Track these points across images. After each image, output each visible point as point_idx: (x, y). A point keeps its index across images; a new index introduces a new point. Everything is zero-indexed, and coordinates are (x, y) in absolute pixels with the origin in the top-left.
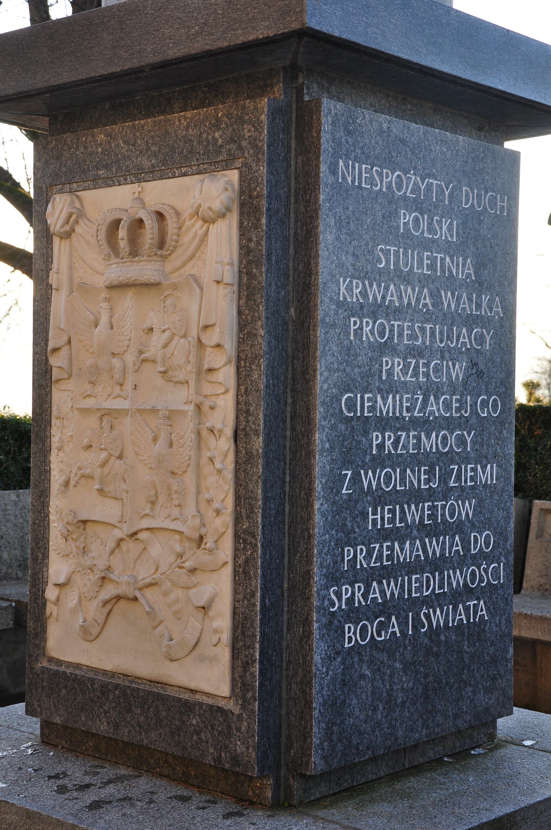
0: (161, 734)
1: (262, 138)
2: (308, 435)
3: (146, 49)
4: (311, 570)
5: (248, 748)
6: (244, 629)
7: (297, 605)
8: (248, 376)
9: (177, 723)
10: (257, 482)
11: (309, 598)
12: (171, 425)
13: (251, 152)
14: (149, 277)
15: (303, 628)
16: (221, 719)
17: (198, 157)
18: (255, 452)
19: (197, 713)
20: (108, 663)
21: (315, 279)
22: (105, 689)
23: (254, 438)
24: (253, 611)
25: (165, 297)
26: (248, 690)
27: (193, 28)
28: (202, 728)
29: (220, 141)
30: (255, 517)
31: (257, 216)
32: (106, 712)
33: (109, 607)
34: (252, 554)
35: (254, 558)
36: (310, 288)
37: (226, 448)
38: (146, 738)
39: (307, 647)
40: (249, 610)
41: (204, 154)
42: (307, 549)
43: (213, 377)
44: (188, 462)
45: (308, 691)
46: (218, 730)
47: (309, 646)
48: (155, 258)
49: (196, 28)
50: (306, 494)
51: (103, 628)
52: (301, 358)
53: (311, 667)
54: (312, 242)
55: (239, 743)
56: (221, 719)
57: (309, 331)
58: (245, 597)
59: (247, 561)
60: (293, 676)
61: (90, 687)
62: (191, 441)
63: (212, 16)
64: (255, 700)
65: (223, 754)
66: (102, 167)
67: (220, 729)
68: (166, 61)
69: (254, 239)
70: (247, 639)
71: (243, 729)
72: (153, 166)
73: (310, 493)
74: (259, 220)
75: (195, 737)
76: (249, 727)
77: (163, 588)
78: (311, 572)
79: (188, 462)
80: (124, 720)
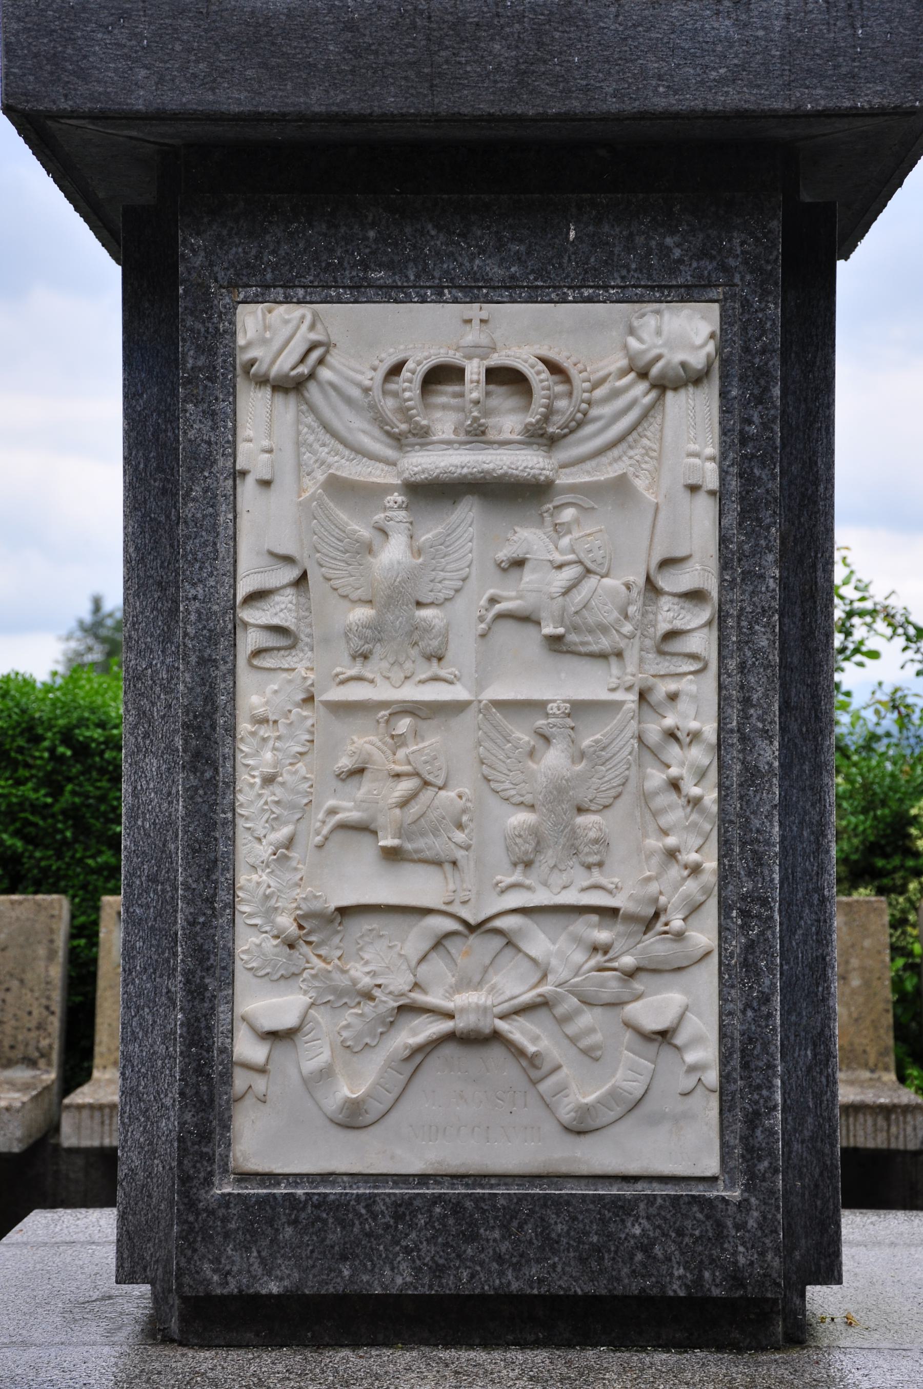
0: (554, 1266)
1: (772, 257)
2: (815, 739)
3: (601, 87)
4: (828, 954)
5: (762, 1254)
6: (747, 1059)
7: (800, 1014)
8: (747, 643)
9: (595, 1239)
10: (769, 816)
11: (824, 1000)
12: (572, 728)
13: (748, 277)
14: (537, 472)
15: (814, 1050)
16: (699, 1216)
17: (624, 272)
18: (764, 768)
19: (642, 1214)
20: (413, 1160)
21: (826, 489)
22: (403, 1210)
23: (762, 744)
24: (767, 1026)
25: (555, 508)
26: (760, 1159)
27: (714, 69)
28: (656, 1238)
29: (677, 253)
30: (766, 872)
31: (763, 382)
32: (407, 1251)
33: (418, 1058)
34: (762, 933)
35: (767, 940)
36: (815, 503)
37: (706, 762)
38: (517, 1279)
39: (824, 1080)
40: (759, 1026)
41: (639, 270)
42: (818, 921)
43: (678, 646)
44: (620, 789)
45: (827, 1150)
46: (692, 1235)
47: (828, 1076)
48: (540, 441)
49: (722, 71)
50: (813, 833)
51: (397, 1100)
52: (799, 614)
53: (833, 1110)
54: (819, 429)
55: (741, 1249)
56: (699, 1216)
57: (815, 572)
58: (748, 1006)
59: (750, 946)
60: (795, 1130)
61: (363, 1211)
62: (630, 754)
63: (758, 57)
64: (776, 1171)
65: (707, 1274)
66: (380, 266)
67: (697, 1233)
68: (646, 112)
69: (756, 419)
70: (754, 1074)
71: (751, 1223)
72: (513, 277)
73: (823, 831)
74: (766, 389)
75: (639, 1256)
76: (765, 1218)
77: (560, 1010)
78: (828, 958)
79: (620, 789)
80: (459, 1256)
